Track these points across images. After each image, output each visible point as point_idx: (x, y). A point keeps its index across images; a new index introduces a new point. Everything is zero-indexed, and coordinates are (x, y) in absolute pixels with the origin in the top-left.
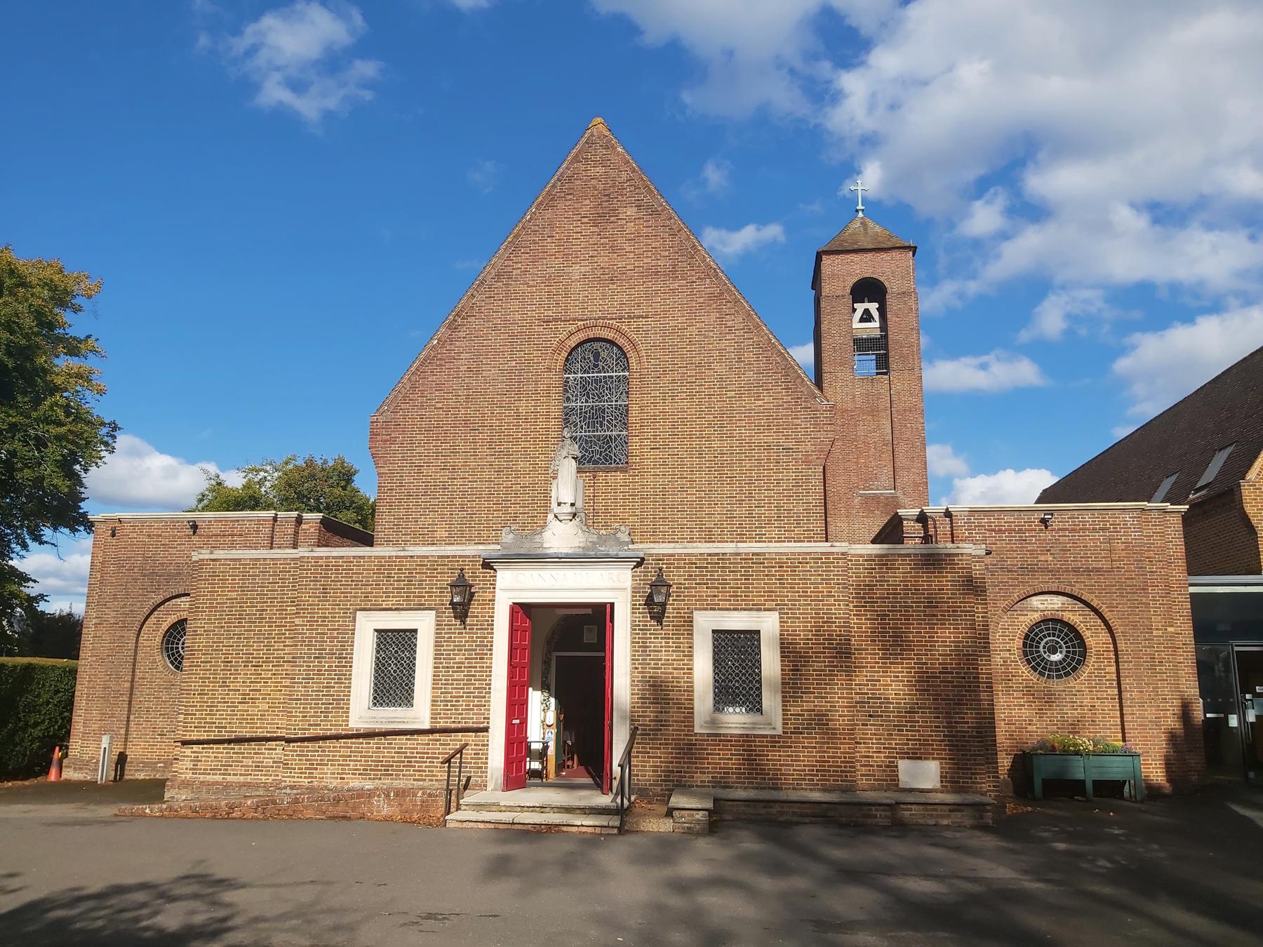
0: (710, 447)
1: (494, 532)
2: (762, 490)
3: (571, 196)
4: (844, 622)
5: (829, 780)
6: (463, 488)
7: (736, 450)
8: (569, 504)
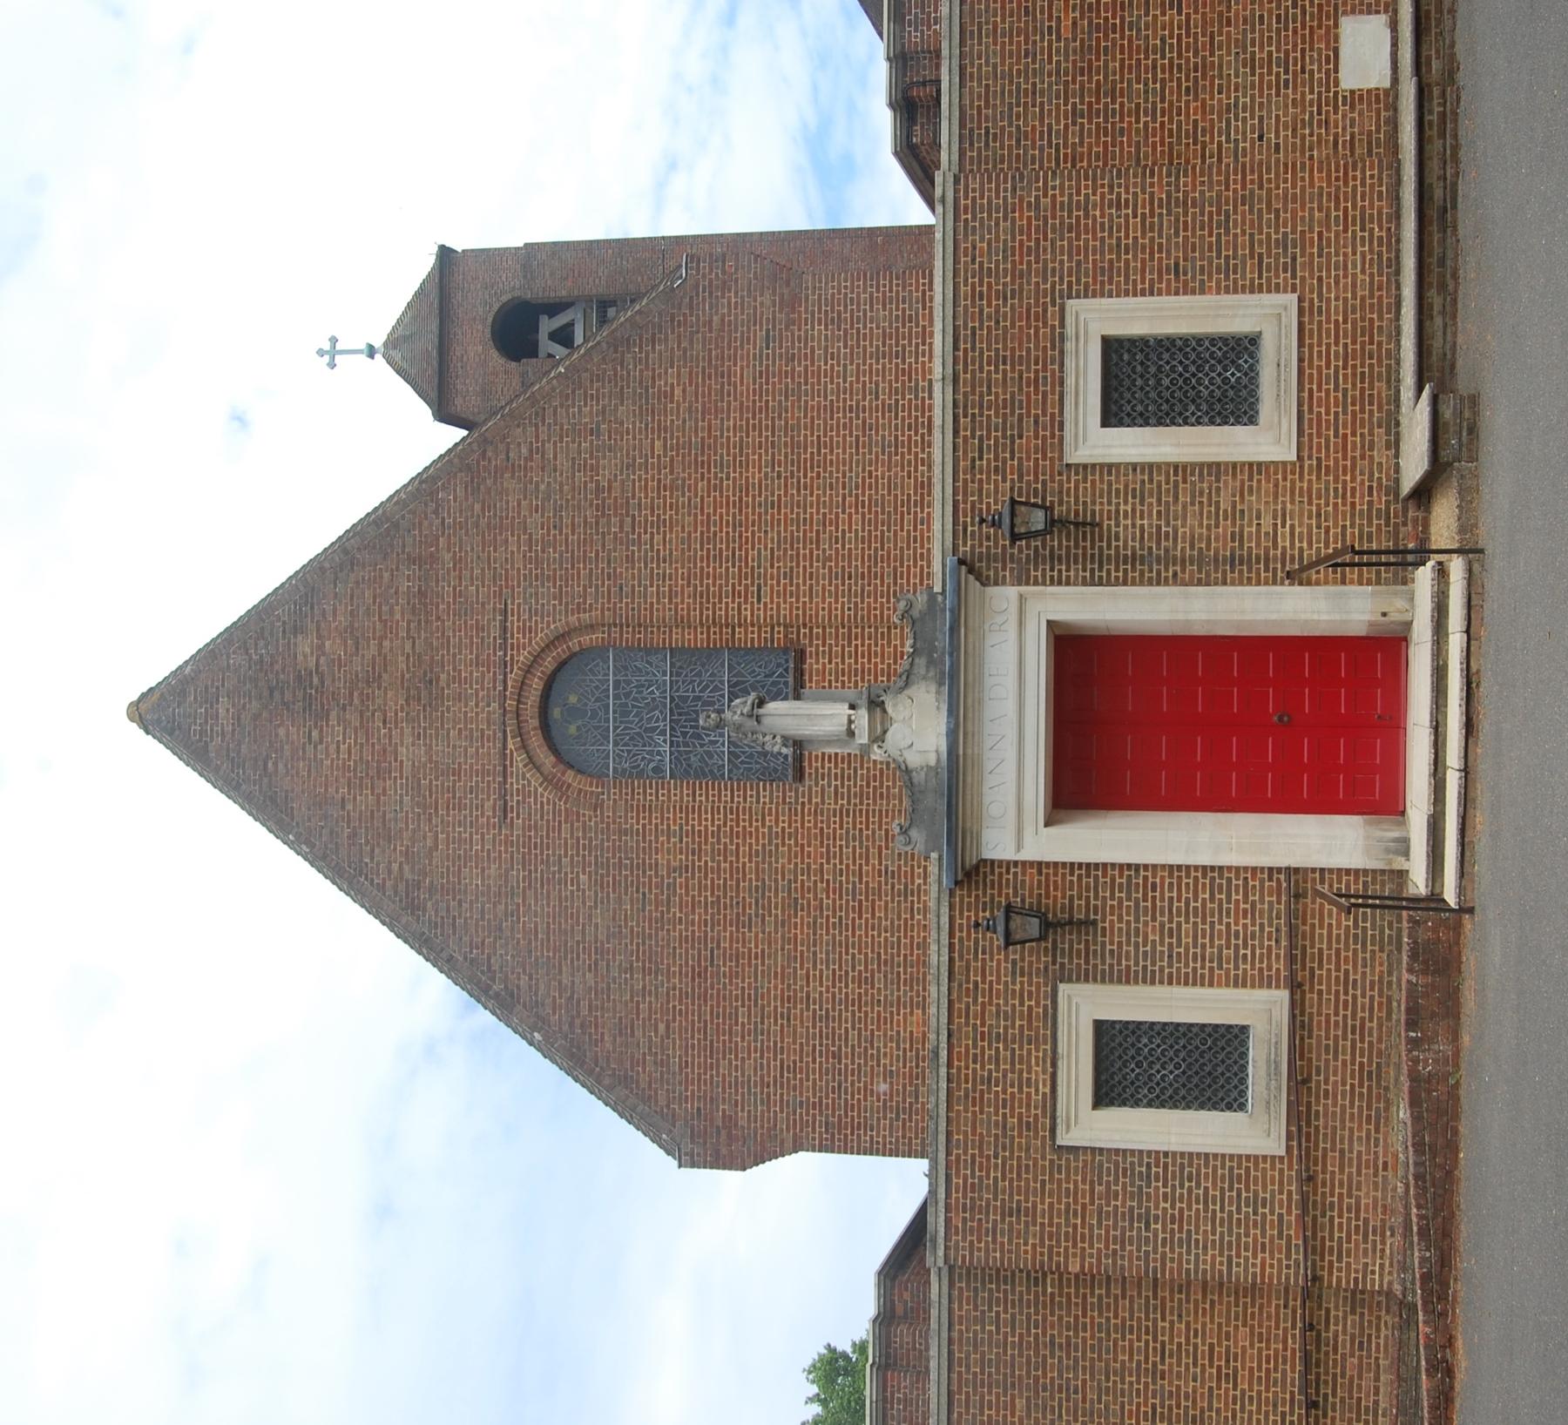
2: (845, 388)
3: (270, 765)
4: (1086, 179)
6: (828, 980)
7: (767, 437)
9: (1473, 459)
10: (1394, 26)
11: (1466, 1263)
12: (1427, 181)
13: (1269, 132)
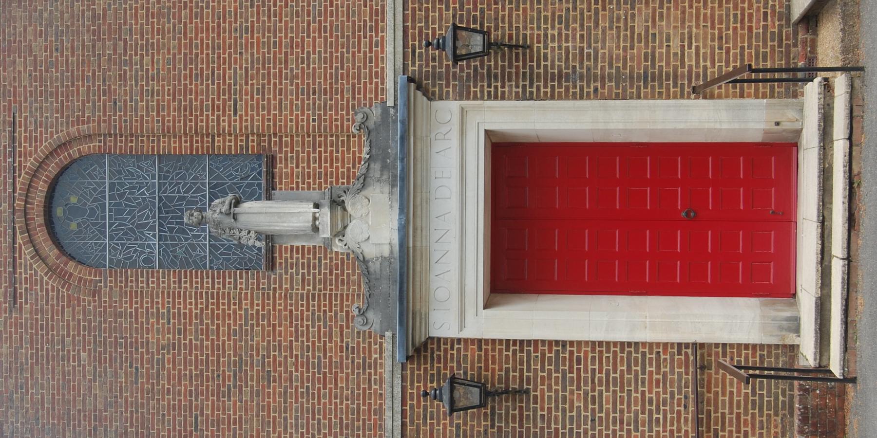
0: (236, 14)
1: (374, 387)
8: (316, 210)
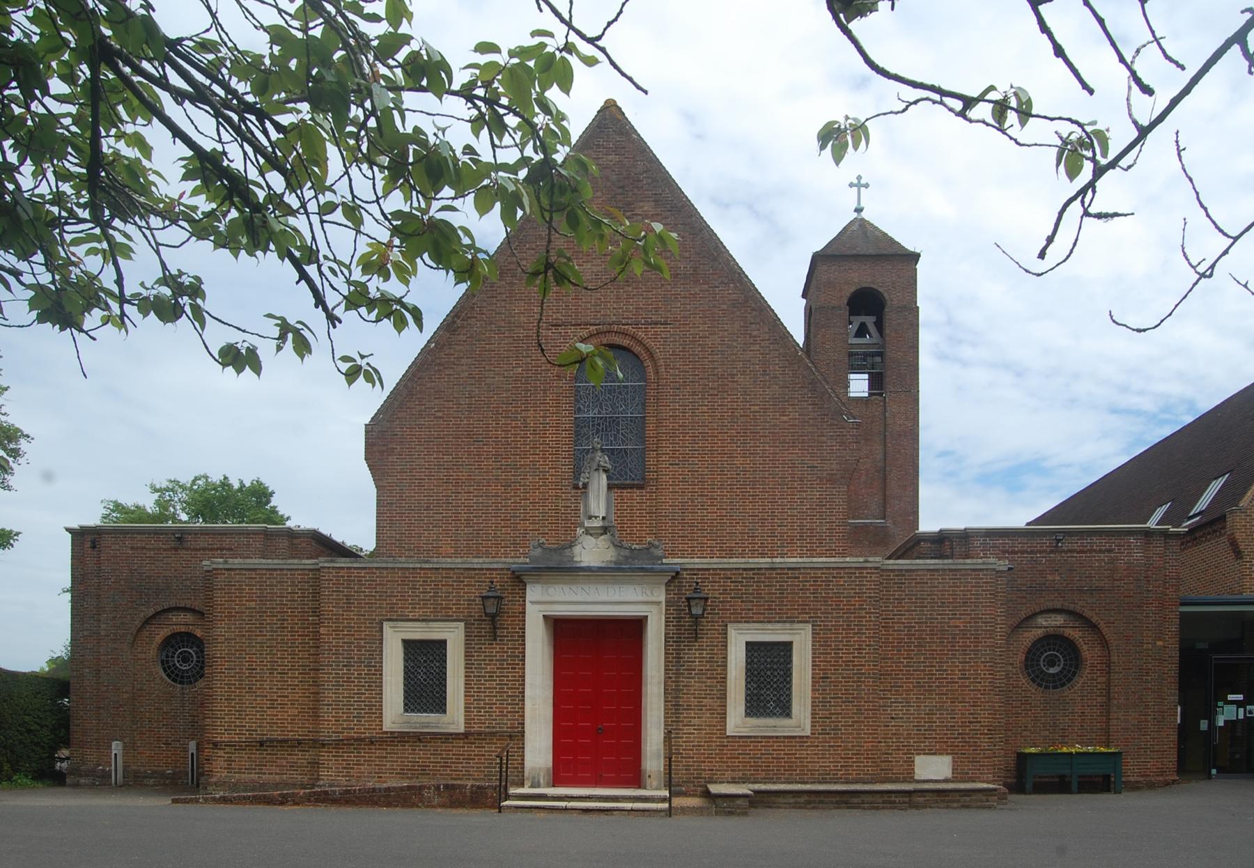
4: (874, 633)
5: (852, 774)
9: (717, 813)
10: (946, 781)
11: (333, 809)
12: (862, 795)
13: (895, 722)
